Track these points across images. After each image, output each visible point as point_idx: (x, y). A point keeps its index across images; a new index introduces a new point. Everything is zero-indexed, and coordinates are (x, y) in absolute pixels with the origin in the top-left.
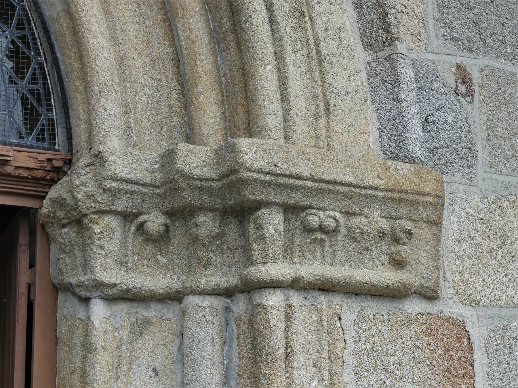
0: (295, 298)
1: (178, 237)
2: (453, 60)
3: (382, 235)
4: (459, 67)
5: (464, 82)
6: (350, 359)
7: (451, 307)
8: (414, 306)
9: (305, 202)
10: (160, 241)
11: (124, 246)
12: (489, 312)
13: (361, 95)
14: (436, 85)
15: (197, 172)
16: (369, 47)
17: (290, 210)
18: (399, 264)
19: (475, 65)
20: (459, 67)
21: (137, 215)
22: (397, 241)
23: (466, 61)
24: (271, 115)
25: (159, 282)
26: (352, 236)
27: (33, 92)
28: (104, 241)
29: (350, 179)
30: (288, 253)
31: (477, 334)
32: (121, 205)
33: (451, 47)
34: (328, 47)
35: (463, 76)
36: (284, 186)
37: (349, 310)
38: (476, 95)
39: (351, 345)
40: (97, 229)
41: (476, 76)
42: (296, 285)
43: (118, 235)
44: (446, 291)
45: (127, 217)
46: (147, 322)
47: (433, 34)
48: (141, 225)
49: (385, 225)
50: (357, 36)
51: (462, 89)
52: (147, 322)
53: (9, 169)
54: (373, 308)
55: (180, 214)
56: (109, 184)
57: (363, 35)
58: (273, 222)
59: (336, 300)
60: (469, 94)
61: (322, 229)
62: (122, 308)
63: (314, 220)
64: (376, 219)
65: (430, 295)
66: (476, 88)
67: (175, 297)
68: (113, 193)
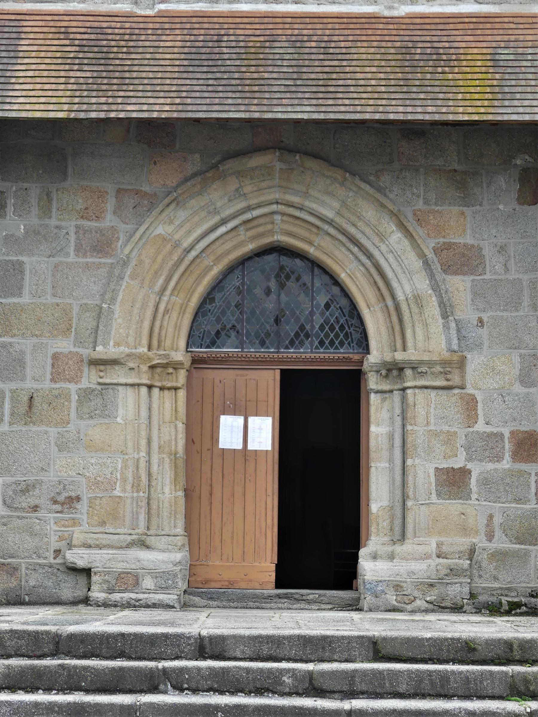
0: (417, 391)
1: (390, 376)
2: (477, 316)
3: (441, 373)
4: (479, 318)
5: (480, 322)
6: (432, 405)
7: (470, 390)
8: (456, 391)
9: (416, 366)
10: (387, 376)
11: (377, 379)
12: (485, 391)
13: (440, 333)
14: (469, 325)
15: (389, 361)
16: (443, 318)
17: (413, 368)
18: (448, 380)
19: (485, 317)
20: (479, 318)
21: (380, 371)
22: (446, 374)
23: (482, 315)
24: (410, 343)
25: (386, 387)
26: (432, 373)
27: (362, 337)
28: (371, 378)
29: (428, 359)
30: (415, 379)
31: (479, 398)
32: (374, 369)
33: (476, 312)
34: (430, 321)
35: (480, 320)
36: (409, 363)
37: (433, 393)
38: (485, 326)
39: (433, 402)
40: (369, 375)
41: (485, 320)
42: (415, 387)
43: (375, 376)
44: (468, 386)
45: (377, 372)
46: (386, 398)
47: (469, 309)
48: (381, 374)
49: (442, 370)
50: (440, 316)
51: (480, 324)
52: (386, 398)
53: (353, 360)
54: (441, 392)
55: (389, 370)
56: (370, 365)
57: (442, 315)
58: (408, 372)
59: (429, 390)
60: (482, 326)
61: (422, 372)
62: (379, 395)
63: (419, 370)
64: (438, 368)
65: (462, 388)
66: (485, 324)
67: (391, 391)
68: (372, 367)
